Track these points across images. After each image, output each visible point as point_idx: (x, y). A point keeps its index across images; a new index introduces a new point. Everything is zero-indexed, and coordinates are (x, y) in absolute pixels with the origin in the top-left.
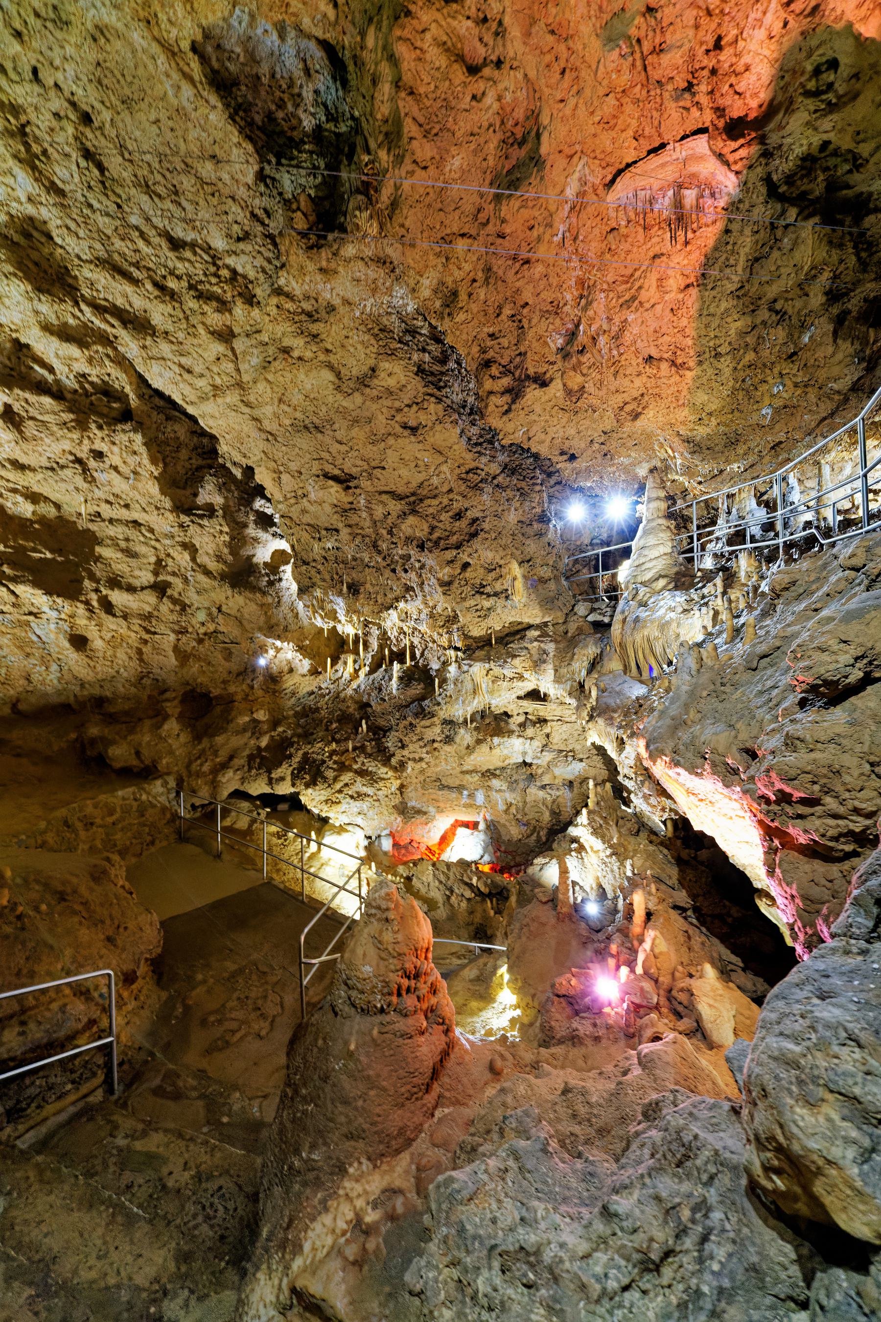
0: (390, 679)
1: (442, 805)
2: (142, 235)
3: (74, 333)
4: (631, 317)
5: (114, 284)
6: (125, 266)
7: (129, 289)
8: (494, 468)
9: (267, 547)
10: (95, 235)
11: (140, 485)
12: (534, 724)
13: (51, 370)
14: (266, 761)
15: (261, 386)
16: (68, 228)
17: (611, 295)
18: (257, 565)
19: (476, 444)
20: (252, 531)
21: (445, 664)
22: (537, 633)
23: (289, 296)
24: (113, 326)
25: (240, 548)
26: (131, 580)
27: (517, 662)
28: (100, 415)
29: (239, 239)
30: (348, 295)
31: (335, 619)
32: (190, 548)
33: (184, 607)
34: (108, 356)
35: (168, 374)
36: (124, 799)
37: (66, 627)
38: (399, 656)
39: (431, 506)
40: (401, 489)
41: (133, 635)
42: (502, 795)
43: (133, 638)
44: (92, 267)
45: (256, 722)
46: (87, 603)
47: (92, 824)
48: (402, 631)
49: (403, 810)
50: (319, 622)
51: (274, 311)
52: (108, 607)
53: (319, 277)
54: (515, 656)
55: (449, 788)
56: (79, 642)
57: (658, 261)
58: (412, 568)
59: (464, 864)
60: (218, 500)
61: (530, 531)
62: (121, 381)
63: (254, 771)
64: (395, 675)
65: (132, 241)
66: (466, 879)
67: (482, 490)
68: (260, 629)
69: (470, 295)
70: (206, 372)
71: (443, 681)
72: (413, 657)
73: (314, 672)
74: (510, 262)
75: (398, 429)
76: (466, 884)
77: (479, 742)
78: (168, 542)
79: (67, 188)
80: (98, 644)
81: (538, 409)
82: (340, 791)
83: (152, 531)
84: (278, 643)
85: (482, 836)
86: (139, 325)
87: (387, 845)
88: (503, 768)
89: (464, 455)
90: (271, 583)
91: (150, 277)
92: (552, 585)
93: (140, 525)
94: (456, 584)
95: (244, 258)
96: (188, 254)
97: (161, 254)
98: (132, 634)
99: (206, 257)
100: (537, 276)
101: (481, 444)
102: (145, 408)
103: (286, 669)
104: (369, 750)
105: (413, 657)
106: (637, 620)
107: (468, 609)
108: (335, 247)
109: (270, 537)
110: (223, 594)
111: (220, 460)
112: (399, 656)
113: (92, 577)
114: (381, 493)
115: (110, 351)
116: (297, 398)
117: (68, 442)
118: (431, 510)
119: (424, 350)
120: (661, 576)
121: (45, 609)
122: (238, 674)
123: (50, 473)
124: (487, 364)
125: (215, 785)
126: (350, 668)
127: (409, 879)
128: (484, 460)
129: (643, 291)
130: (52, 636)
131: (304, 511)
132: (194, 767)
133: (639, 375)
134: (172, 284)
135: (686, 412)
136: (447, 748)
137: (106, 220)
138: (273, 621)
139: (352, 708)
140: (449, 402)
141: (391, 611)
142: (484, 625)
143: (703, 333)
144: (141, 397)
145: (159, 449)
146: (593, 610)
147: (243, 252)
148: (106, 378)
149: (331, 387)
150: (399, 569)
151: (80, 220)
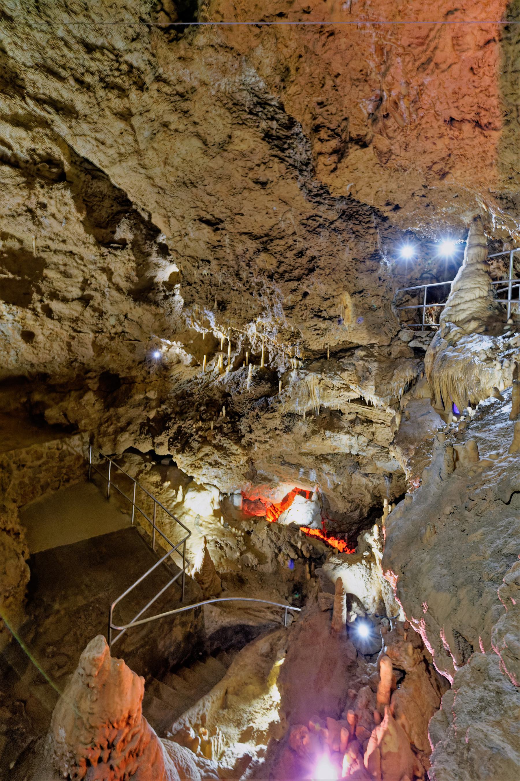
0: (246, 377)
1: (284, 477)
2: (66, 44)
3: (22, 120)
4: (427, 80)
5: (49, 82)
6: (56, 68)
7: (58, 84)
8: (332, 215)
9: (166, 271)
10: (35, 47)
11: (70, 227)
12: (363, 422)
13: (10, 147)
14: (154, 428)
15: (150, 153)
16: (16, 44)
17: (408, 58)
18: (157, 284)
19: (316, 195)
20: (154, 258)
21: (289, 369)
22: (363, 353)
23: (165, 81)
24: (49, 113)
25: (146, 271)
26: (66, 294)
27: (345, 375)
28: (43, 177)
29: (133, 40)
30: (205, 78)
31: (209, 327)
32: (107, 271)
33: (101, 314)
34: (46, 135)
35: (88, 146)
36: (49, 448)
37: (19, 326)
38: (255, 360)
39: (278, 246)
40: (257, 231)
41: (65, 333)
42: (331, 478)
43: (65, 336)
44: (33, 70)
45: (147, 398)
46: (34, 310)
47: (23, 466)
48: (259, 340)
49: (253, 476)
50: (198, 329)
51: (155, 94)
52: (49, 312)
53: (179, 64)
54: (344, 370)
55: (290, 464)
56: (28, 336)
57: (451, 17)
58: (265, 293)
59: (294, 528)
60: (129, 236)
61: (362, 267)
62: (57, 152)
63: (143, 436)
64: (250, 375)
65: (59, 48)
66: (293, 542)
67: (319, 234)
68: (155, 332)
69: (297, 69)
70: (114, 144)
71: (286, 384)
72: (266, 360)
73: (195, 364)
74: (317, 36)
75: (251, 184)
76: (292, 546)
77: (314, 432)
78: (91, 267)
79: (14, 14)
80: (40, 338)
81: (361, 167)
82: (201, 459)
83: (82, 259)
84: (169, 342)
85: (313, 506)
86: (67, 111)
87: (238, 501)
88: (336, 454)
89: (305, 204)
90: (166, 297)
91: (73, 75)
92: (381, 313)
93: (74, 254)
94: (297, 309)
95: (136, 54)
96: (98, 55)
97: (79, 56)
98: (64, 331)
99: (112, 56)
100: (343, 47)
101: (320, 195)
102: (76, 172)
103: (175, 360)
104: (225, 430)
105: (266, 360)
106: (444, 358)
107: (308, 328)
108: (190, 37)
109: (168, 263)
110: (127, 305)
111: (134, 207)
112: (255, 360)
113: (39, 291)
114: (241, 234)
115: (48, 132)
116: (177, 161)
117: (20, 198)
118: (279, 249)
119: (272, 119)
120: (474, 319)
121: (5, 313)
122: (140, 363)
123: (11, 219)
124: (317, 129)
125: (115, 443)
126: (220, 364)
127: (249, 533)
128: (322, 208)
129: (438, 52)
130: (10, 332)
131: (186, 246)
132: (103, 428)
133: (441, 136)
134: (88, 79)
135: (494, 171)
136: (285, 436)
137: (41, 35)
138: (165, 326)
139: (217, 396)
140: (291, 161)
141: (251, 324)
142: (322, 340)
143: (509, 91)
144: (73, 163)
145: (86, 202)
146: (415, 337)
147: (135, 50)
148: (49, 151)
149: (200, 152)
150: (255, 293)
151: (23, 37)
